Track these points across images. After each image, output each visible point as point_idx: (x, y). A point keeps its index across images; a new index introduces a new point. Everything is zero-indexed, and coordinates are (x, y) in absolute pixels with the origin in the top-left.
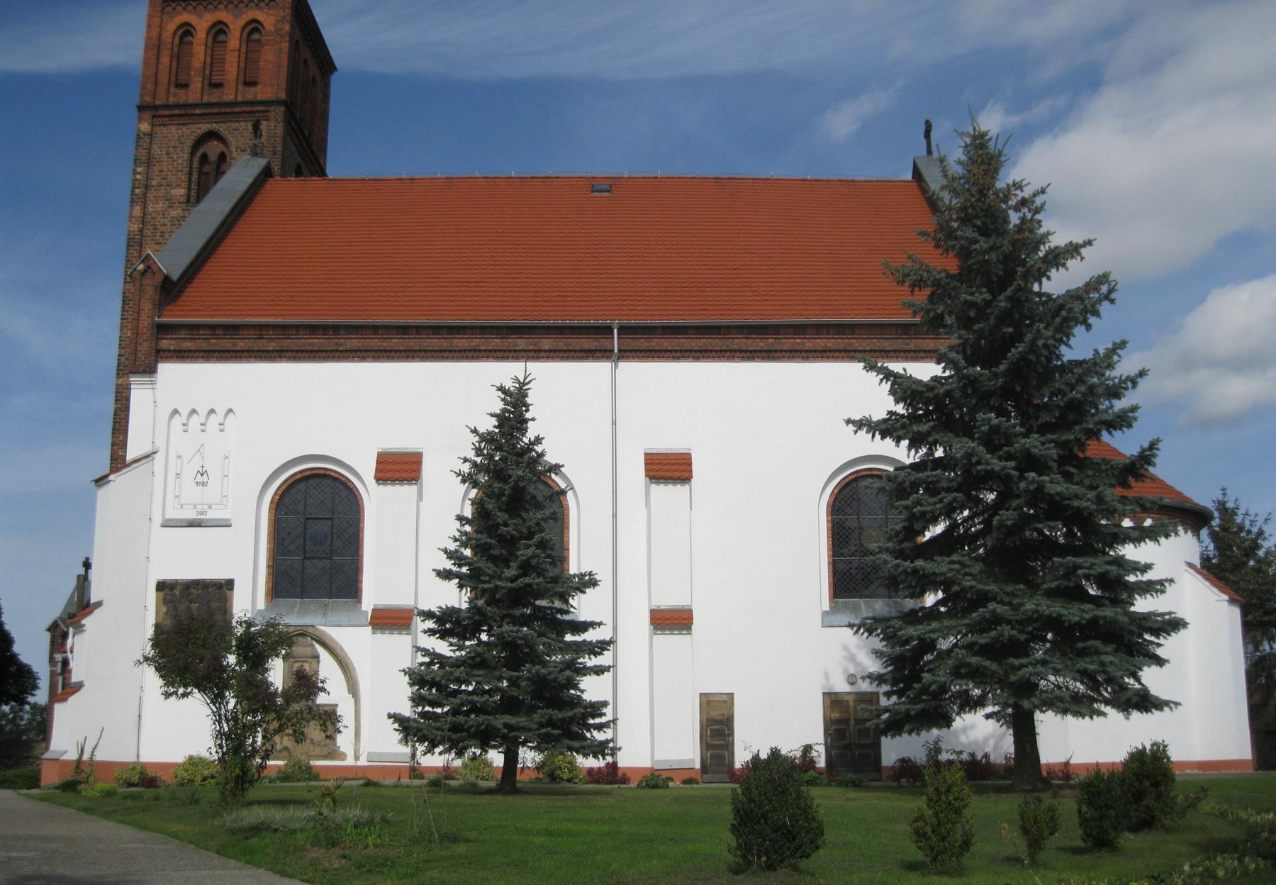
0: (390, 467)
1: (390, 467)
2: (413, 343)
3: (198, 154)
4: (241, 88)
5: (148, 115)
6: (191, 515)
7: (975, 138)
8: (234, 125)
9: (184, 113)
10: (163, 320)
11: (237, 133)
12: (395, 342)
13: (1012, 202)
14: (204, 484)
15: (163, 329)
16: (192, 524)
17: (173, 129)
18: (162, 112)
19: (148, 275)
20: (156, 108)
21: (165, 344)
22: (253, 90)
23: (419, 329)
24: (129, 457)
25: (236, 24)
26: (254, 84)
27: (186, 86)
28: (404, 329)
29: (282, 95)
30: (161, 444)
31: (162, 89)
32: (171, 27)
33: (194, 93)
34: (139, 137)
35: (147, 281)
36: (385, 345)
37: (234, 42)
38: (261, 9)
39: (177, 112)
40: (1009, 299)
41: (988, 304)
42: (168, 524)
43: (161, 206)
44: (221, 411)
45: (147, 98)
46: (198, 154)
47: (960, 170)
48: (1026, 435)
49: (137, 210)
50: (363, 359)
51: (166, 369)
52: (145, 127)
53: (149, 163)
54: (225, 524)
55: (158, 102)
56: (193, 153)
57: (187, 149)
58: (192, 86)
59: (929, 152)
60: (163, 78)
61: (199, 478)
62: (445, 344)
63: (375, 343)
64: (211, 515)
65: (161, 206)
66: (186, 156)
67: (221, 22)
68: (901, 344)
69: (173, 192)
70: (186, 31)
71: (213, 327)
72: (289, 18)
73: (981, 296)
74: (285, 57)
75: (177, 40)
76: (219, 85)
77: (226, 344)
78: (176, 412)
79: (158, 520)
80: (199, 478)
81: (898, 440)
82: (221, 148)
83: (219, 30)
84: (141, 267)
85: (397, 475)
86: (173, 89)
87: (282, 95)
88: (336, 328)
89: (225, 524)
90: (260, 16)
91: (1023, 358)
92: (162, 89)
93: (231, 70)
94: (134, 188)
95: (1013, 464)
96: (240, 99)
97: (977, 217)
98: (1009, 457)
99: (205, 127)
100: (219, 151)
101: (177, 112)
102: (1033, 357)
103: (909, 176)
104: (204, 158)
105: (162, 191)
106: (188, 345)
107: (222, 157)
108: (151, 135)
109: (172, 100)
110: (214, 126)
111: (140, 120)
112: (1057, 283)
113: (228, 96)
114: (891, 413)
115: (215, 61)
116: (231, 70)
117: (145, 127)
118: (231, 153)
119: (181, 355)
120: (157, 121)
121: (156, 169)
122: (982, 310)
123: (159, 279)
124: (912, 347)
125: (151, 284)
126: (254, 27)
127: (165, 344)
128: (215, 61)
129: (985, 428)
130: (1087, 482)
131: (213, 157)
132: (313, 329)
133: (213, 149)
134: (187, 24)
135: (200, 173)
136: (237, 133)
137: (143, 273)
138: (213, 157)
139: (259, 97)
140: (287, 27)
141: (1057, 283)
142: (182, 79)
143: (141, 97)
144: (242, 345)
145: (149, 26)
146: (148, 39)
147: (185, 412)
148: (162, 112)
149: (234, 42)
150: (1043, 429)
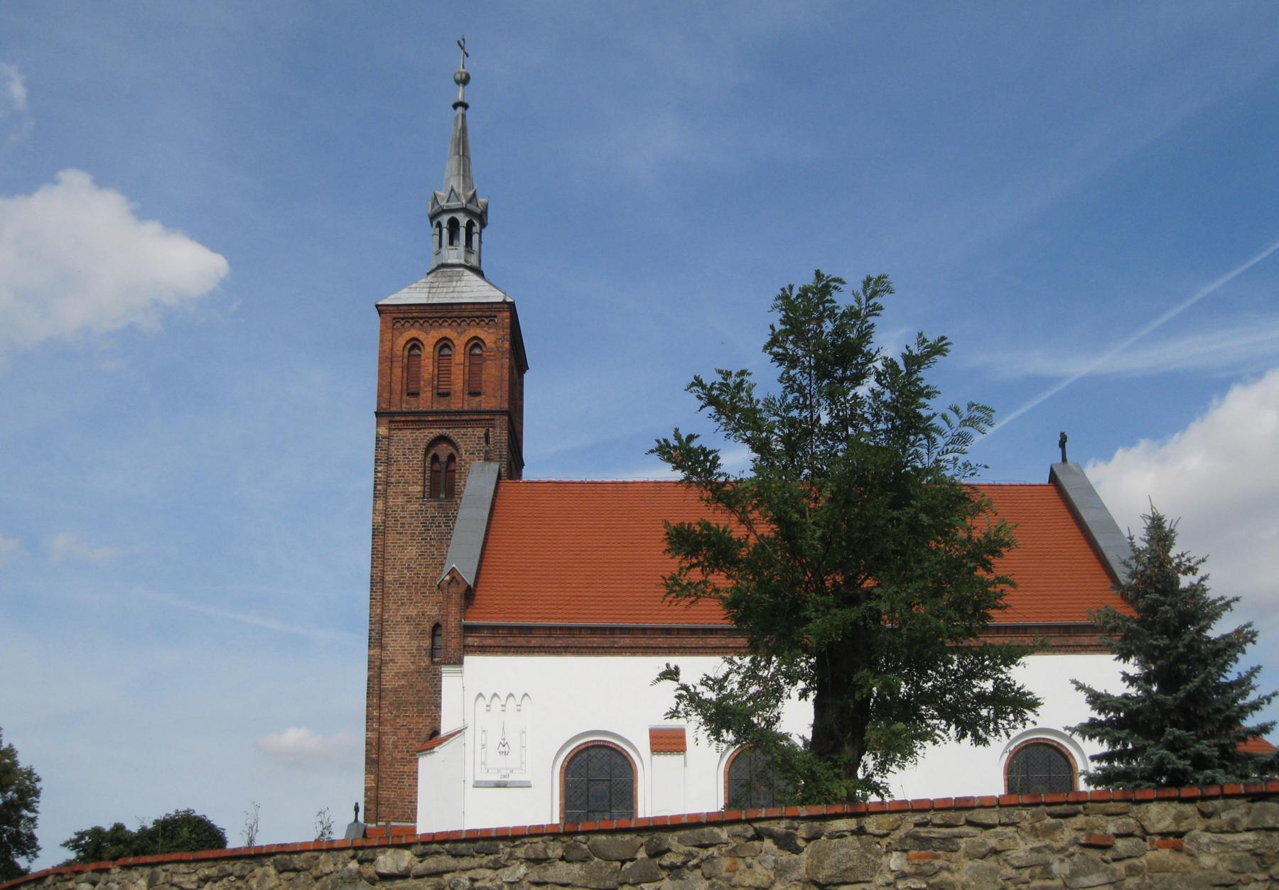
0: (661, 741)
1: (661, 741)
2: (675, 641)
3: (430, 455)
4: (466, 397)
5: (385, 420)
6: (496, 778)
7: (1153, 519)
8: (463, 431)
9: (417, 419)
10: (468, 622)
11: (468, 439)
12: (660, 641)
13: (1182, 568)
14: (506, 753)
15: (468, 629)
16: (498, 785)
17: (408, 432)
18: (397, 418)
19: (454, 584)
20: (393, 414)
21: (470, 641)
22: (477, 399)
23: (679, 631)
24: (445, 729)
25: (459, 340)
26: (478, 394)
27: (416, 394)
28: (668, 631)
29: (505, 406)
30: (469, 722)
31: (396, 397)
32: (401, 341)
33: (426, 401)
34: (378, 440)
35: (452, 590)
36: (652, 642)
37: (459, 356)
38: (482, 327)
39: (412, 418)
40: (1186, 646)
41: (1167, 647)
42: (478, 785)
43: (400, 501)
44: (518, 696)
45: (384, 406)
46: (430, 455)
47: (1145, 545)
48: (1197, 742)
49: (380, 505)
50: (634, 654)
51: (473, 662)
52: (383, 431)
53: (388, 462)
54: (526, 785)
55: (393, 409)
56: (426, 454)
57: (421, 452)
58: (422, 395)
59: (1064, 460)
60: (397, 387)
61: (501, 749)
62: (701, 643)
63: (644, 641)
64: (513, 778)
65: (400, 501)
66: (421, 457)
67: (445, 338)
68: (1063, 641)
69: (410, 488)
70: (415, 344)
71: (510, 628)
72: (508, 337)
73: (1164, 642)
74: (506, 371)
75: (406, 353)
76: (447, 394)
77: (521, 641)
78: (480, 695)
79: (470, 783)
80: (501, 749)
81: (1101, 741)
82: (450, 450)
83: (444, 344)
84: (448, 578)
85: (669, 747)
86: (405, 397)
87: (505, 406)
88: (612, 630)
89: (526, 785)
90: (482, 334)
91: (1197, 689)
92: (396, 397)
93: (458, 380)
94: (376, 485)
95: (1188, 762)
96: (466, 408)
97: (1158, 582)
98: (1184, 757)
99: (436, 432)
100: (448, 452)
101: (412, 418)
102: (1204, 689)
103: (1045, 480)
104: (435, 458)
105: (400, 488)
106: (490, 642)
107: (451, 458)
108: (388, 438)
109: (405, 408)
110: (445, 431)
111: (378, 425)
112: (1217, 630)
113: (456, 406)
114: (1092, 719)
115: (443, 368)
116: (458, 380)
117: (383, 431)
118: (460, 456)
119: (483, 650)
120: (393, 426)
121: (394, 468)
122: (1163, 651)
123: (462, 589)
124: (1071, 643)
125: (456, 594)
126: (476, 343)
127: (470, 641)
128: (443, 368)
129: (1170, 738)
130: (1238, 772)
131: (443, 458)
132: (593, 630)
133: (443, 451)
134: (415, 339)
135: (432, 471)
136: (468, 439)
137: (449, 583)
138: (443, 458)
139: (484, 407)
140: (507, 345)
141: (1217, 630)
142: (413, 388)
143: (378, 404)
144: (534, 642)
145: (382, 341)
146: (382, 352)
147: (488, 695)
148: (397, 418)
149: (459, 356)
150: (1206, 737)
